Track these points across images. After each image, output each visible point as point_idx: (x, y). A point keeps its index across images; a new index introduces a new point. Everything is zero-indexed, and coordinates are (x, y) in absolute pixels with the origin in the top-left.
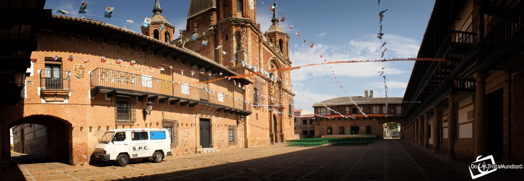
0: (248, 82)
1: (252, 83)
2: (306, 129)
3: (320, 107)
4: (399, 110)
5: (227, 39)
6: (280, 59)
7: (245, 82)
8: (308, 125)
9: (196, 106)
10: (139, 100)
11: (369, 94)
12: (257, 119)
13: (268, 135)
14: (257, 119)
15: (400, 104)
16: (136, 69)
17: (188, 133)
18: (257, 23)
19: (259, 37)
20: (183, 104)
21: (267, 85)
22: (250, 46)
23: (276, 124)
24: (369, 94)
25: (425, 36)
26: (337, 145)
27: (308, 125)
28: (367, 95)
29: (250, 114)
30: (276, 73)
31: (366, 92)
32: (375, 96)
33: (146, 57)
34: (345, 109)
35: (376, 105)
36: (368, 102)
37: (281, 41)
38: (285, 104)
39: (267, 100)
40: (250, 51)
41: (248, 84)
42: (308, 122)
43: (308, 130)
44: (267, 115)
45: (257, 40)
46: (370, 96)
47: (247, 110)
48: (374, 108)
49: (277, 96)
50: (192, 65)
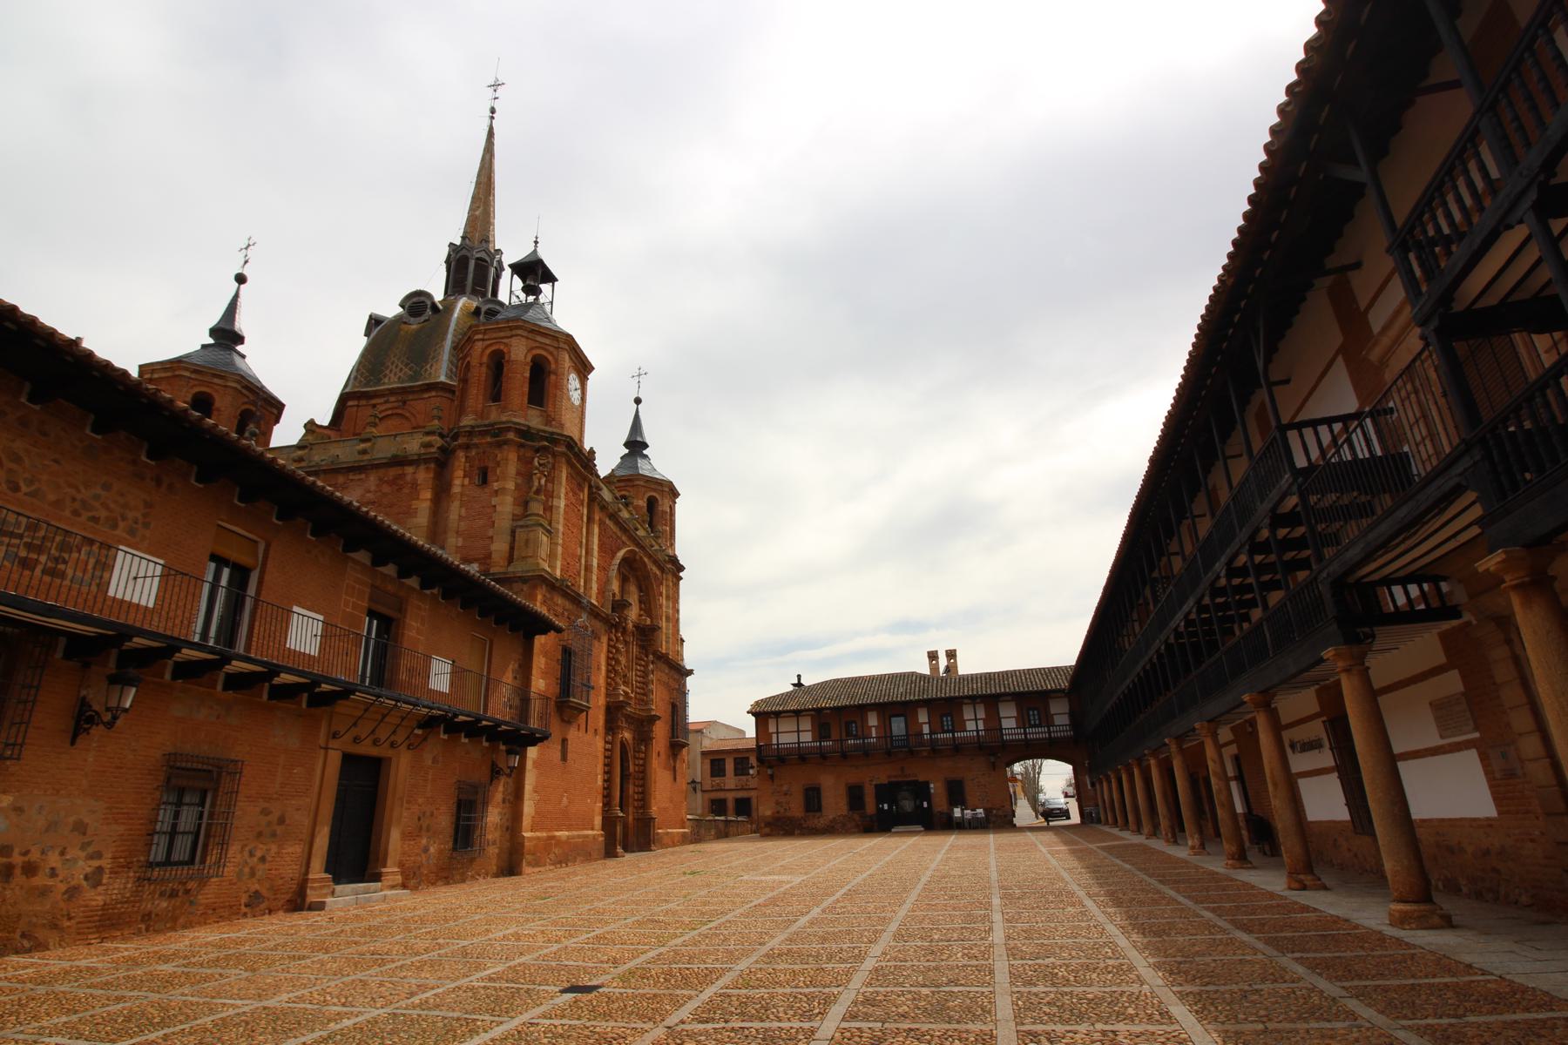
0: (545, 626)
1: (559, 630)
2: (720, 795)
3: (777, 715)
4: (1060, 715)
5: (484, 481)
6: (650, 557)
7: (530, 626)
8: (730, 780)
9: (341, 707)
10: (68, 655)
11: (943, 662)
12: (564, 758)
13: (598, 820)
14: (564, 758)
15: (1061, 691)
16: (95, 519)
17: (281, 821)
18: (587, 447)
19: (590, 487)
20: (286, 693)
21: (604, 639)
22: (562, 510)
23: (625, 776)
24: (943, 662)
25: (1152, 460)
26: (1182, 830)
27: (730, 780)
28: (935, 668)
29: (545, 738)
30: (633, 598)
31: (933, 656)
32: (964, 668)
33: (159, 482)
34: (864, 720)
35: (973, 699)
36: (948, 692)
37: (652, 503)
38: (659, 703)
39: (603, 690)
40: (561, 528)
41: (544, 632)
42: (730, 766)
43: (730, 797)
44: (599, 744)
45: (585, 495)
46: (948, 669)
47: (534, 723)
48: (968, 714)
49: (633, 676)
50: (351, 546)
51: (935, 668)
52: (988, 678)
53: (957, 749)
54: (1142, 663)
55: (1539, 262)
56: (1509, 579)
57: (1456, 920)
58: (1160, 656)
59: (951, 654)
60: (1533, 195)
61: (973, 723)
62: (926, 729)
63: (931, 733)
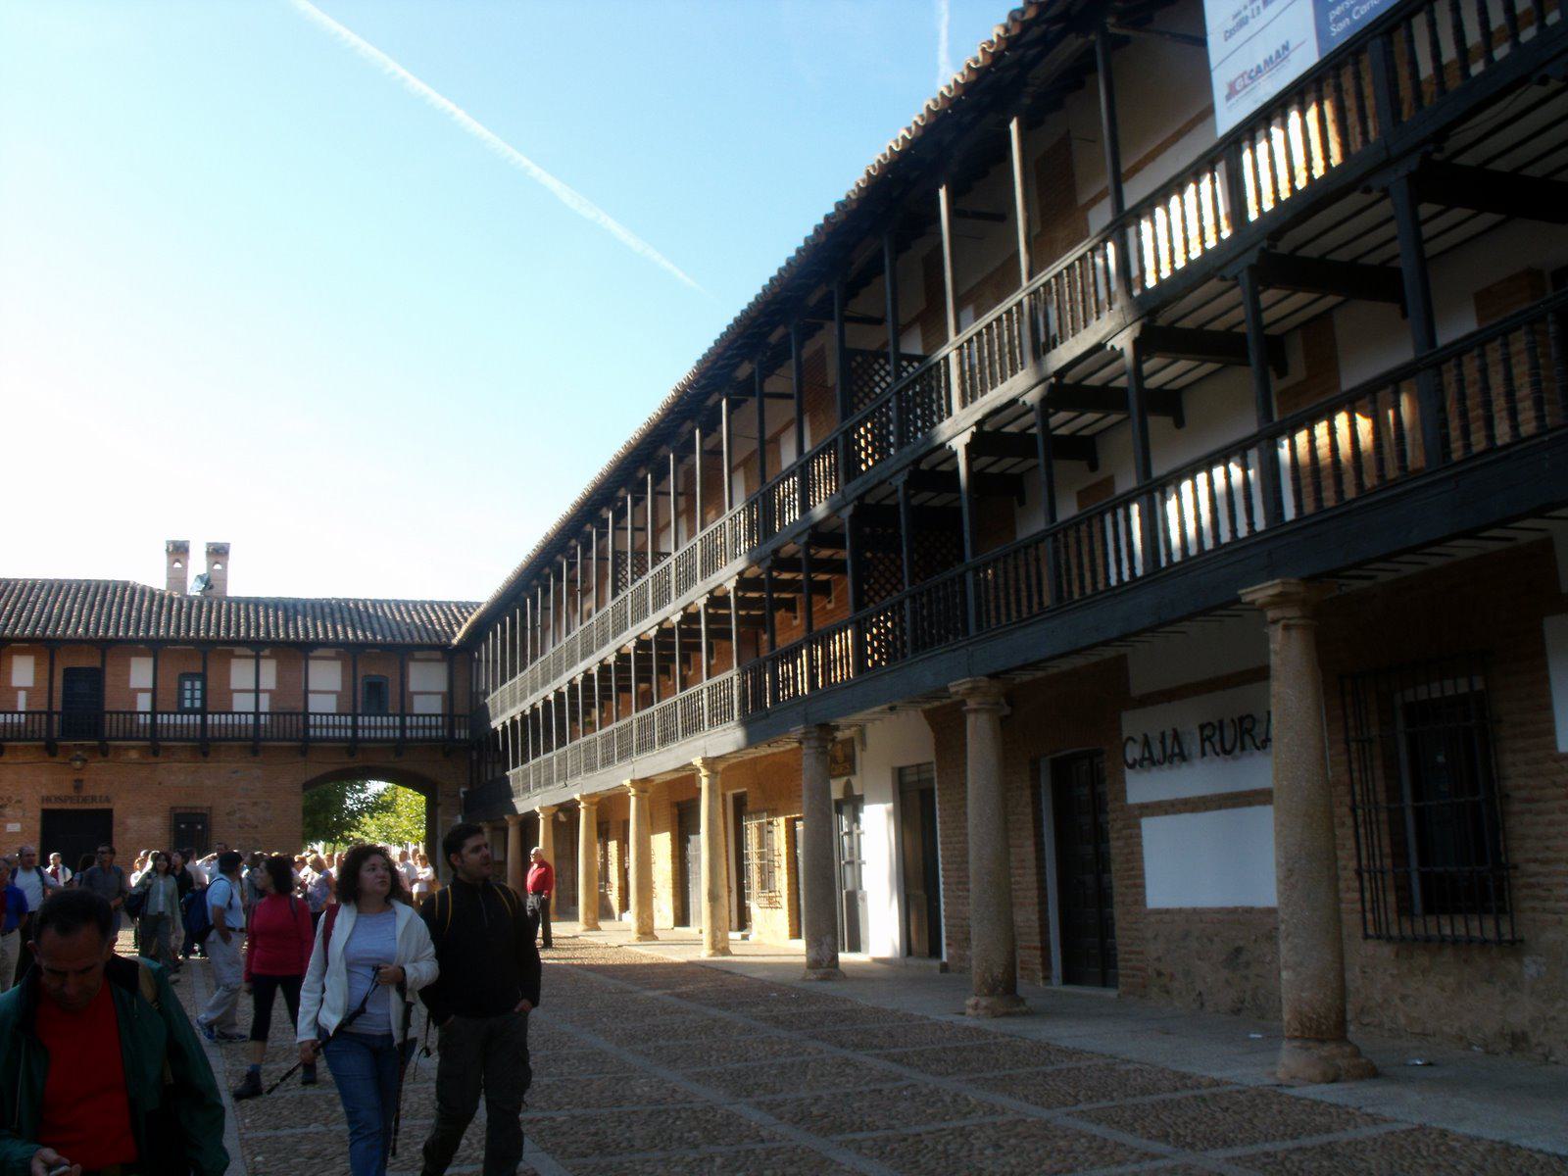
11: (197, 564)
24: (197, 564)
28: (177, 579)
31: (179, 551)
32: (241, 583)
35: (257, 648)
46: (208, 583)
48: (241, 674)
51: (177, 579)
52: (290, 609)
53: (204, 745)
54: (531, 700)
55: (1393, 239)
56: (971, 704)
57: (1264, 737)
58: (573, 687)
59: (218, 552)
60: (1413, 162)
61: (248, 688)
62: (144, 703)
63: (154, 713)
